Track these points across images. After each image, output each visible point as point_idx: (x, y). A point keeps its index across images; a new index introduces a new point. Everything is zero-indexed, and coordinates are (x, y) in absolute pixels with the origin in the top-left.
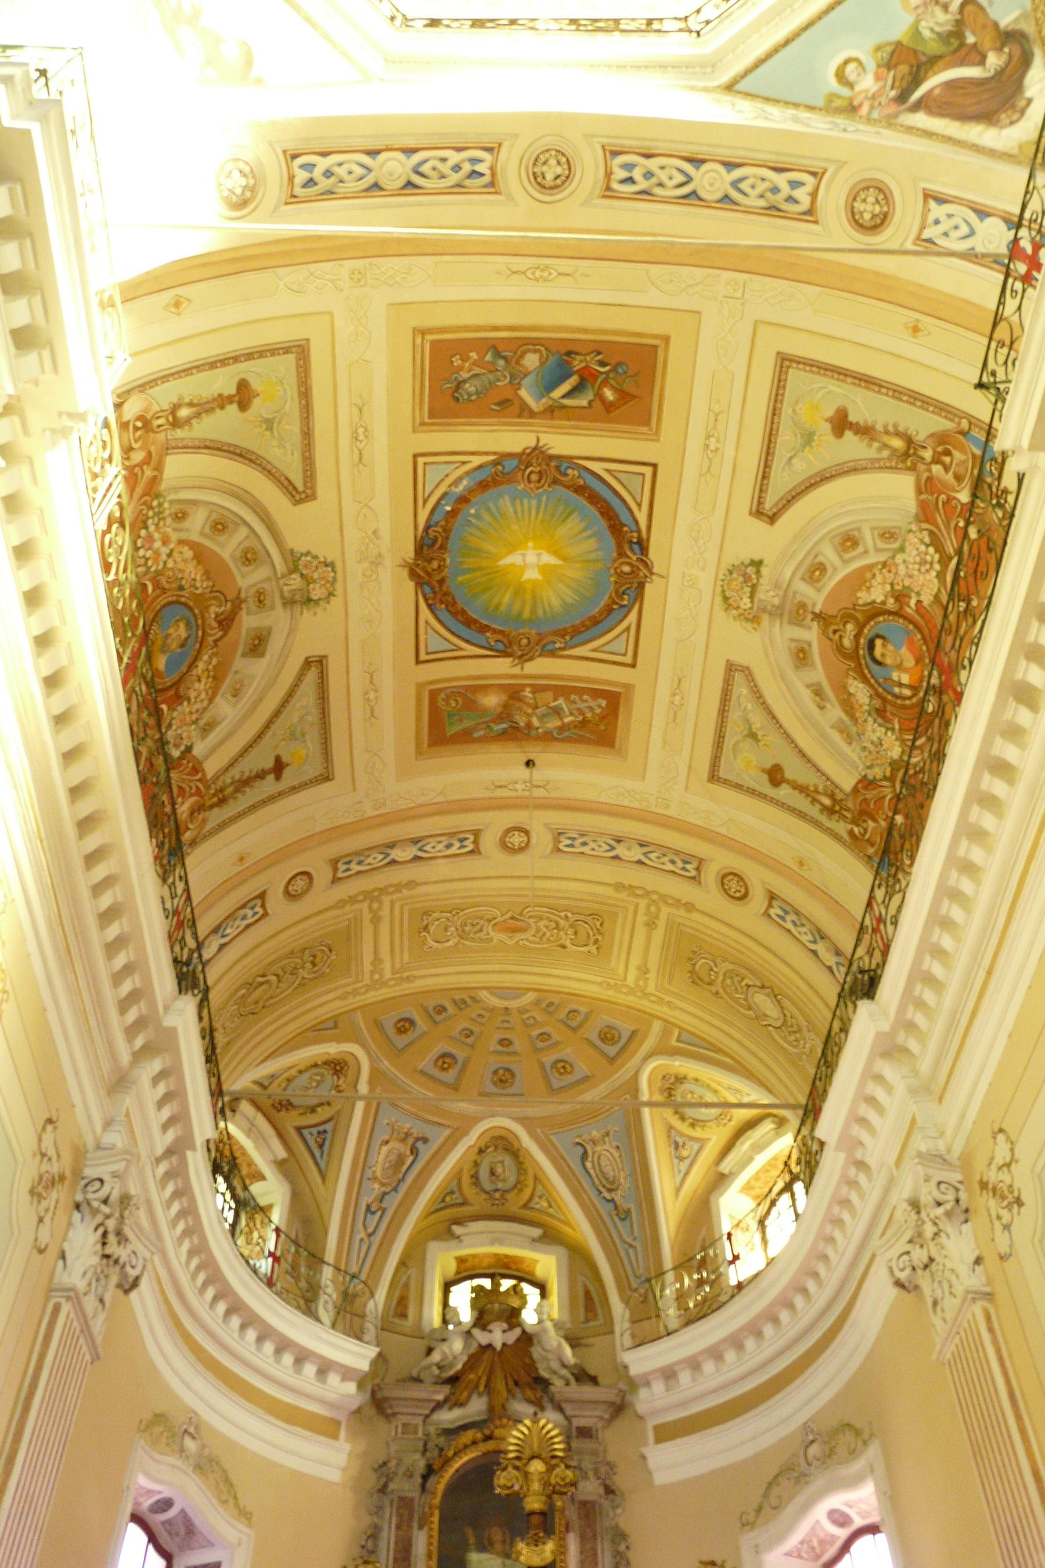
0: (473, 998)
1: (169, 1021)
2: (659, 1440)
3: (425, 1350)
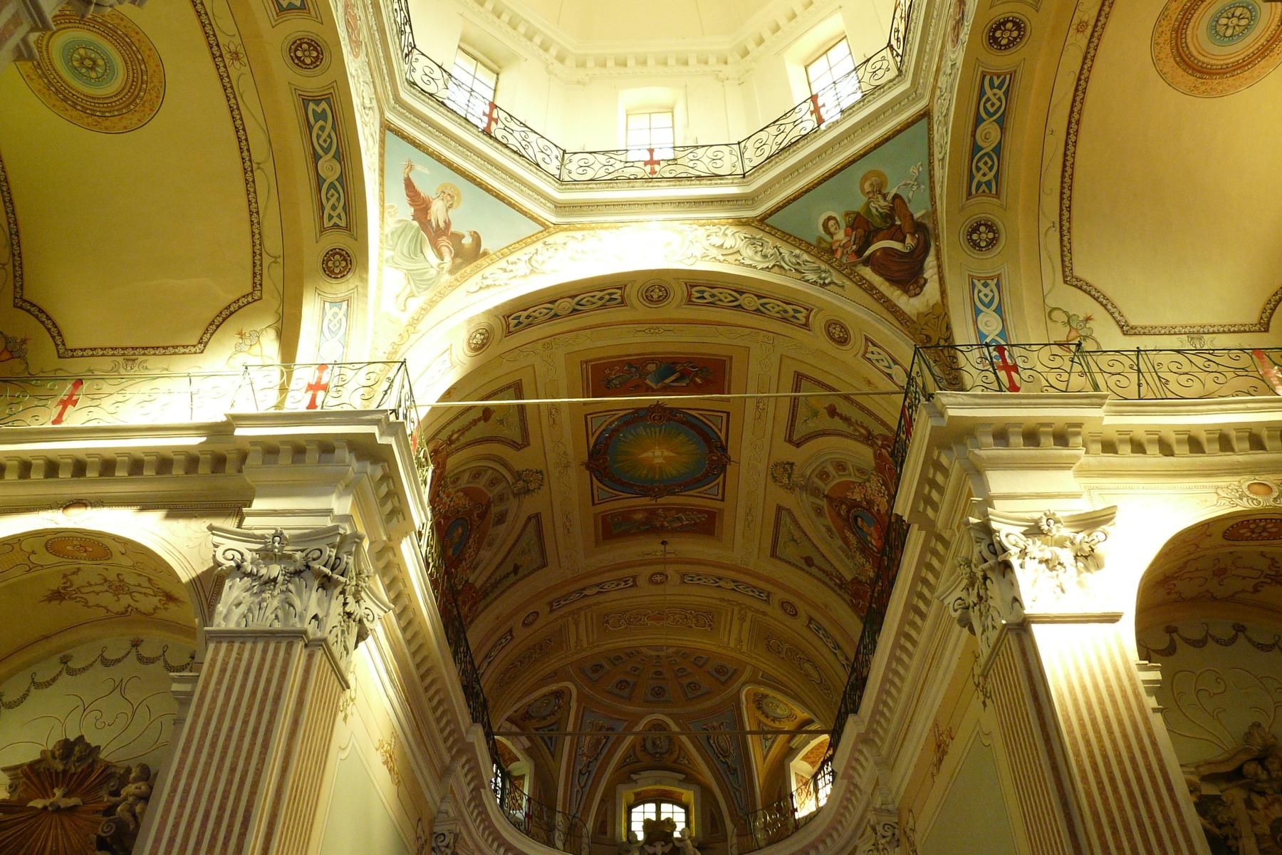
1: (470, 739)
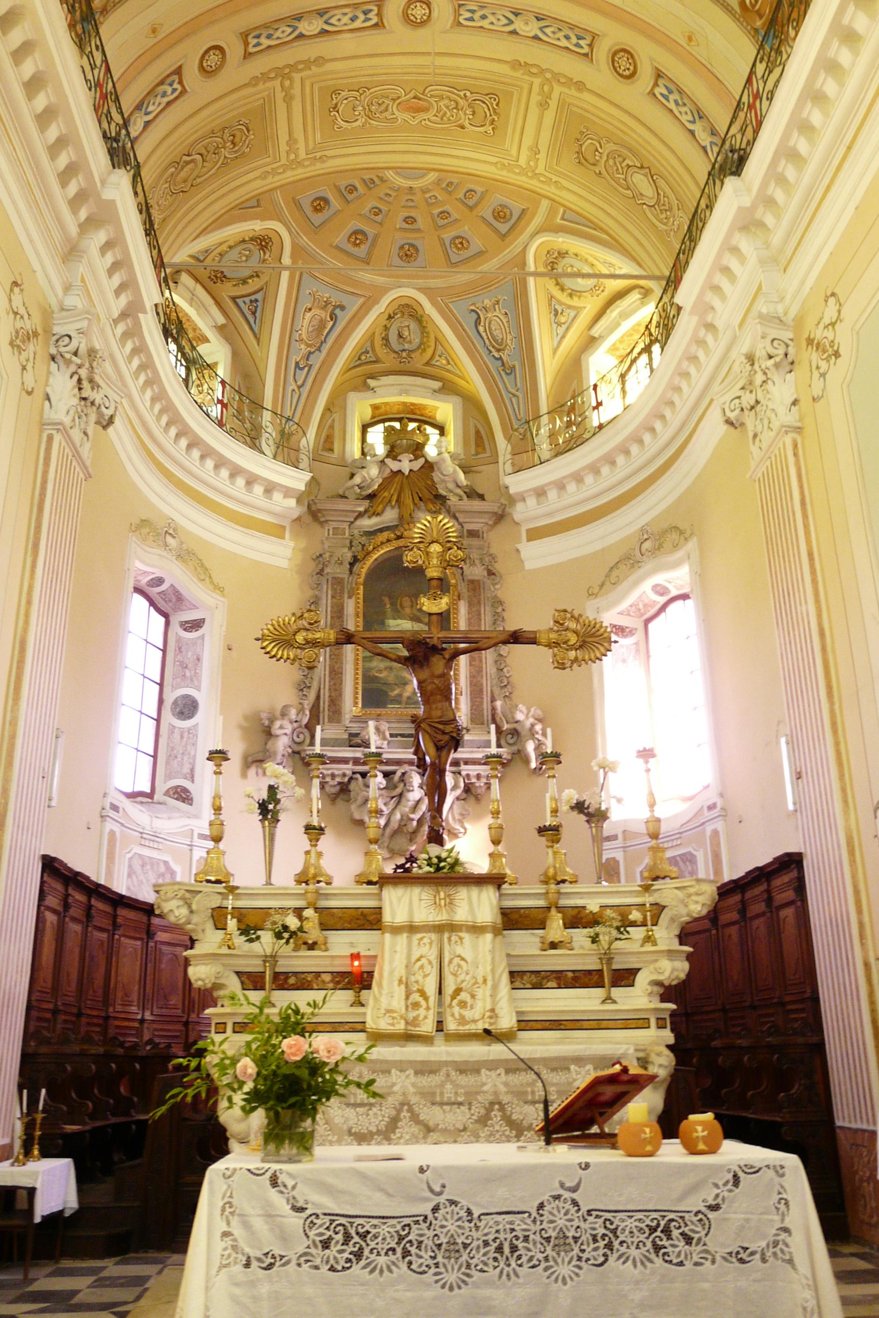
0: (381, 179)
1: (108, 194)
2: (529, 540)
3: (349, 476)
